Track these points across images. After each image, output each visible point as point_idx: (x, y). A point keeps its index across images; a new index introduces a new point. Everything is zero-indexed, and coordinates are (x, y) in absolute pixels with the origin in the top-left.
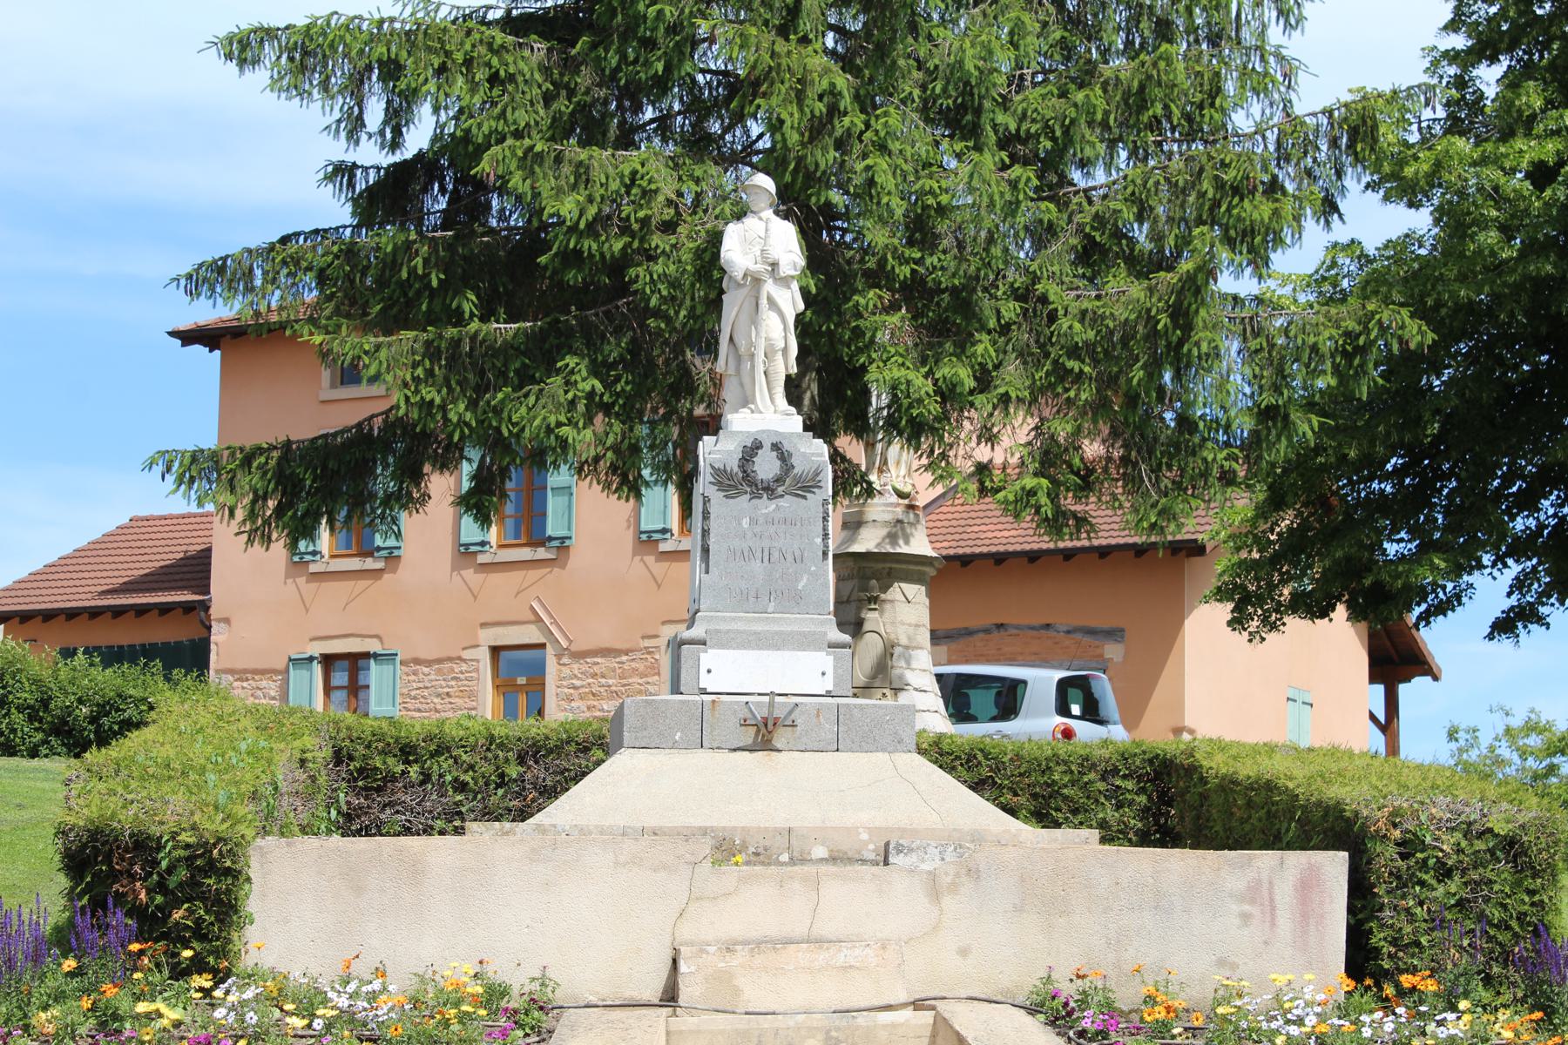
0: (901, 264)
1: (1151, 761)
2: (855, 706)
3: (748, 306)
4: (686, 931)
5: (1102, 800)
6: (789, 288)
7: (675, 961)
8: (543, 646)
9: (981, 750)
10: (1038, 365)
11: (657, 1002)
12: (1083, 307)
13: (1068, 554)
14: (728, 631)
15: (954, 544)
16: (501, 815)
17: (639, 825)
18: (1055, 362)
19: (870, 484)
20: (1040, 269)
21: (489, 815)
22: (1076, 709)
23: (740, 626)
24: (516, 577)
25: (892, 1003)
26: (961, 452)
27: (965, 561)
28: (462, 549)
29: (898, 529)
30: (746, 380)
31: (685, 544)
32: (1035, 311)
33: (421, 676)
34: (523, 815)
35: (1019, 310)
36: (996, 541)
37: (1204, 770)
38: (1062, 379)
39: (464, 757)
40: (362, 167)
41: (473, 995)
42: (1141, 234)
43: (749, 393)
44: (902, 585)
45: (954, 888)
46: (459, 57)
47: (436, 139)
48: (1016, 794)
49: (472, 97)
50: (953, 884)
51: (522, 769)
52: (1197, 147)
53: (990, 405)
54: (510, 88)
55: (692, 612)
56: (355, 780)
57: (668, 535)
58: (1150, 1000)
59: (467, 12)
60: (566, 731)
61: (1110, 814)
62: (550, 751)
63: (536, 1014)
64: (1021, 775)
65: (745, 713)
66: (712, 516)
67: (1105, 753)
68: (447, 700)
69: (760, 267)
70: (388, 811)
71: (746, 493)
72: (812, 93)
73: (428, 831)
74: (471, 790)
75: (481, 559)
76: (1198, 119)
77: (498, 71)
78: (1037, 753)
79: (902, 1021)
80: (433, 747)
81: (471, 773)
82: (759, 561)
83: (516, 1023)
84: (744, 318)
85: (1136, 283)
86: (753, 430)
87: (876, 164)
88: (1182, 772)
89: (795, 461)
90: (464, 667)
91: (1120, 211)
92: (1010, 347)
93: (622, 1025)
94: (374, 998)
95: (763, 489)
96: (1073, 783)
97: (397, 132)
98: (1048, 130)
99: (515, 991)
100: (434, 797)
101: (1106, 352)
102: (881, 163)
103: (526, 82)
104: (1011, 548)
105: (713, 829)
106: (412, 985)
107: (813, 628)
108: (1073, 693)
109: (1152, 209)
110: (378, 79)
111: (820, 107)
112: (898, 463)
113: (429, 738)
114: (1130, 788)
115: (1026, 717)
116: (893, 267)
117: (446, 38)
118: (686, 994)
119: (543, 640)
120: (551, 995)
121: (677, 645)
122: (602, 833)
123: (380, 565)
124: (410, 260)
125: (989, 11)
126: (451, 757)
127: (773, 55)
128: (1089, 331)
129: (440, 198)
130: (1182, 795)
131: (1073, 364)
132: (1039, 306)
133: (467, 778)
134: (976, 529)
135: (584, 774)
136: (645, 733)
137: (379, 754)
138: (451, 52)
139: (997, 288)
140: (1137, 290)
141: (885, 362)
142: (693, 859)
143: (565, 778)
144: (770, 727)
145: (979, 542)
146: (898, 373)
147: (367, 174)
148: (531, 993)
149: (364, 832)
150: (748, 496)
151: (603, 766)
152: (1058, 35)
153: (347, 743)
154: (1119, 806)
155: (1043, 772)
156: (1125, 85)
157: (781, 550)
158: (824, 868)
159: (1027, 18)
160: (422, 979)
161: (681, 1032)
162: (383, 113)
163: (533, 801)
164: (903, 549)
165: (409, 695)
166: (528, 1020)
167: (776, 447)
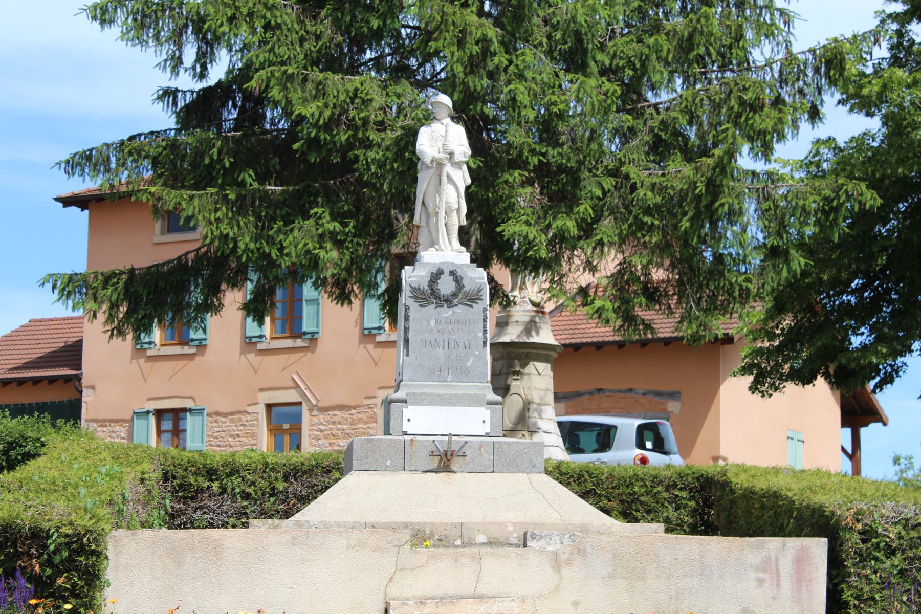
1: (698, 479)
2: (504, 442)
3: (434, 180)
4: (394, 591)
5: (666, 504)
6: (461, 169)
8: (300, 404)
9: (587, 472)
12: (654, 181)
14: (422, 394)
15: (569, 336)
16: (273, 515)
17: (363, 521)
18: (636, 217)
21: (265, 514)
22: (649, 445)
24: (282, 358)
28: (247, 340)
30: (433, 229)
31: (393, 337)
33: (220, 424)
34: (287, 515)
36: (597, 335)
37: (733, 485)
39: (249, 477)
40: (182, 91)
43: (435, 238)
45: (569, 562)
46: (245, 11)
47: (229, 72)
48: (610, 501)
50: (569, 559)
51: (286, 485)
54: (278, 32)
55: (398, 381)
56: (177, 492)
61: (671, 513)
62: (305, 473)
64: (613, 488)
66: (411, 319)
68: (238, 439)
69: (442, 156)
70: (198, 512)
71: (433, 303)
73: (225, 525)
74: (253, 499)
75: (260, 347)
76: (728, 55)
77: (270, 21)
78: (624, 474)
80: (228, 470)
81: (253, 487)
82: (441, 348)
84: (431, 189)
86: (438, 262)
88: (719, 486)
89: (465, 282)
90: (249, 417)
95: (444, 301)
96: (647, 493)
97: (204, 67)
100: (229, 503)
103: (289, 30)
107: (477, 392)
108: (647, 434)
110: (192, 33)
114: (684, 496)
116: (527, 157)
119: (300, 400)
122: (339, 526)
123: (193, 351)
128: (657, 197)
130: (719, 501)
133: (250, 490)
135: (327, 488)
136: (367, 461)
137: (193, 475)
140: (688, 170)
144: (449, 456)
145: (586, 335)
147: (185, 95)
149: (183, 526)
150: (434, 306)
151: (340, 482)
153: (172, 467)
154: (677, 508)
157: (456, 341)
158: (485, 549)
163: (294, 505)
165: (212, 436)
167: (452, 273)
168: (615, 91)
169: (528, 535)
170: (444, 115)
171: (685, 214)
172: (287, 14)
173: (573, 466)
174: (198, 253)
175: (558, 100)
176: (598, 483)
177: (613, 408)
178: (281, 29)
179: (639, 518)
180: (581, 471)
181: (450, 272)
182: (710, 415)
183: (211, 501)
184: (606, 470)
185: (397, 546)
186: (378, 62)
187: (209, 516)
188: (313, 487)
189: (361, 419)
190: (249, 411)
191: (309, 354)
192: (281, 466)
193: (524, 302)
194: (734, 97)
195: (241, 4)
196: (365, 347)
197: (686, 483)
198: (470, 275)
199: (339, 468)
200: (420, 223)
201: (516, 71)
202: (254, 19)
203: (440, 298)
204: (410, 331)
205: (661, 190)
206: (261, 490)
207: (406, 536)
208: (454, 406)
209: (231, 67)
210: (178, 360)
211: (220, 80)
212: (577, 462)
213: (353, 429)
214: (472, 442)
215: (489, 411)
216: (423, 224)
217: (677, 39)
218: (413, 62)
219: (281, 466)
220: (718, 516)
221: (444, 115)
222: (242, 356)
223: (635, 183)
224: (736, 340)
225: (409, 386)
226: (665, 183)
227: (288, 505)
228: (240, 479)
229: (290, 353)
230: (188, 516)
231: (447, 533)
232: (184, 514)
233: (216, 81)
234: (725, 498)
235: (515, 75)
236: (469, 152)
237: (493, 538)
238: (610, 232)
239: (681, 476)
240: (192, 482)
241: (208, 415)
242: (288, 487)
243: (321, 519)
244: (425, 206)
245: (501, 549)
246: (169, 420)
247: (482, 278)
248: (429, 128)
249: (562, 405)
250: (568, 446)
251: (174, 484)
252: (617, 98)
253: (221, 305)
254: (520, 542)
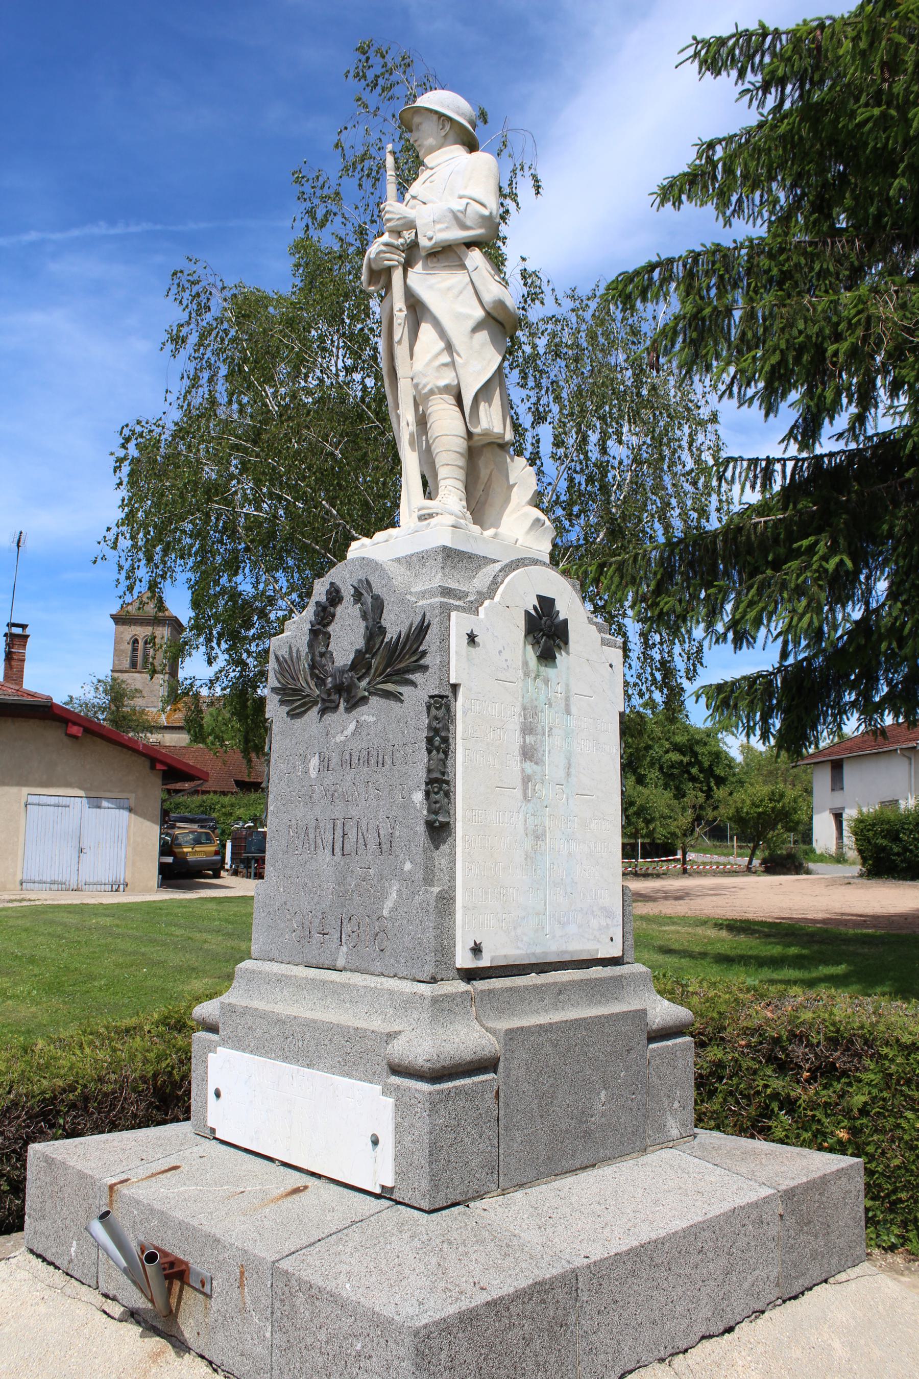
82: (328, 851)
215: (391, 1101)
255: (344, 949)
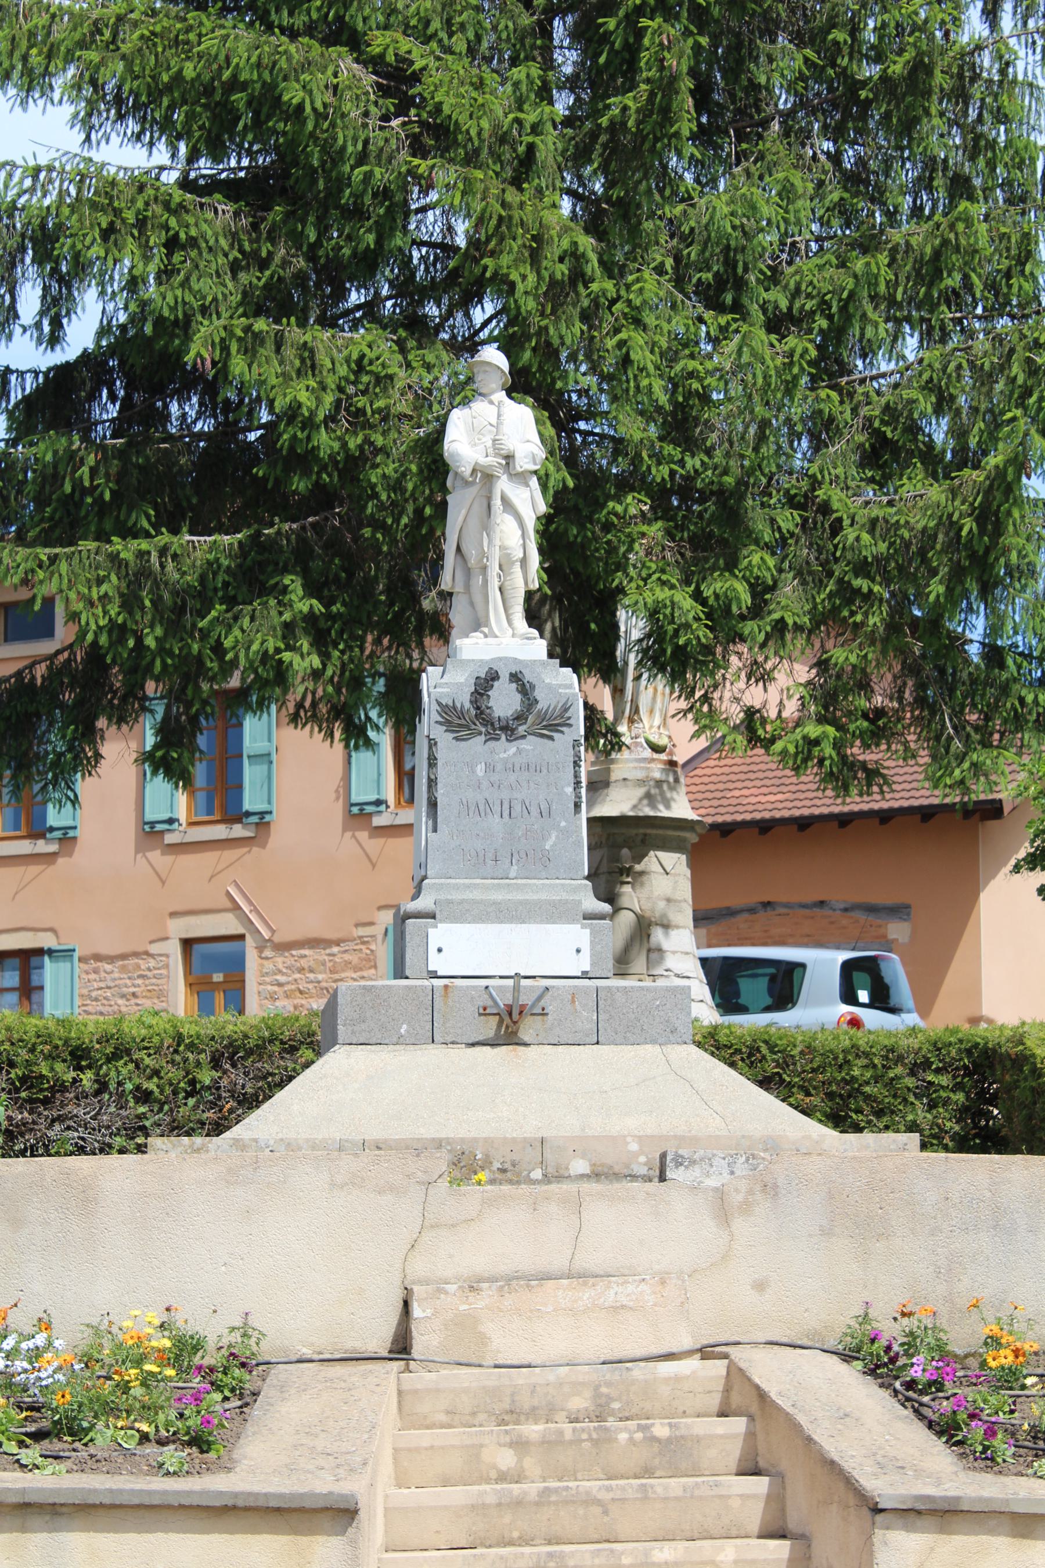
0: (659, 463)
1: (969, 1052)
2: (618, 988)
3: (479, 508)
4: (419, 1267)
5: (912, 1099)
6: (528, 486)
7: (406, 1304)
8: (241, 937)
9: (766, 1042)
10: (820, 585)
11: (386, 1354)
12: (873, 515)
13: (844, 820)
14: (462, 902)
15: (712, 811)
16: (193, 1130)
17: (359, 1138)
18: (840, 581)
19: (617, 735)
20: (821, 471)
21: (177, 1128)
22: (863, 996)
23: (476, 895)
24: (209, 858)
25: (675, 1350)
26: (727, 695)
27: (725, 830)
28: (147, 828)
29: (656, 791)
30: (478, 599)
31: (406, 816)
32: (815, 523)
33: (103, 974)
34: (218, 1128)
35: (798, 520)
36: (760, 807)
37: (1038, 1060)
38: (850, 602)
39: (147, 1061)
40: (17, 371)
41: (159, 1351)
42: (939, 431)
43: (481, 613)
44: (660, 854)
45: (746, 1208)
46: (130, 216)
47: (103, 331)
48: (808, 1094)
49: (146, 265)
50: (746, 1202)
51: (216, 1074)
52: (1003, 323)
53: (763, 634)
54: (194, 254)
55: (416, 881)
56: (17, 1090)
57: (383, 807)
58: (993, 1342)
59: (136, 173)
60: (268, 1028)
61: (921, 1114)
62: (250, 1052)
63: (237, 1373)
64: (813, 1070)
65: (484, 1000)
66: (440, 763)
67: (911, 1041)
68: (133, 1001)
69: (492, 460)
70: (57, 1127)
71: (480, 733)
72: (552, 253)
73: (105, 1149)
74: (159, 1101)
75: (169, 839)
76: (1005, 290)
77: (177, 234)
78: (833, 1045)
79: (688, 1372)
80: (109, 1050)
81: (155, 1080)
82: (497, 816)
83: (212, 1384)
84: (473, 523)
85: (936, 485)
86: (487, 657)
87: (630, 337)
88: (1008, 1064)
89: (538, 694)
90: (152, 963)
91: (914, 401)
92: (786, 565)
93: (343, 1385)
94: (38, 1357)
95: (501, 729)
96: (877, 1079)
97: (57, 324)
98: (824, 305)
99: (211, 1344)
100: (112, 1109)
101: (900, 568)
102: (637, 338)
103: (210, 249)
104: (778, 815)
105: (448, 1141)
106: (84, 1339)
107: (564, 896)
108: (858, 977)
109: (952, 398)
110: (33, 261)
111: (562, 270)
112: (651, 711)
113: (105, 1039)
114: (944, 1083)
115: (805, 1006)
116: (649, 467)
117: (115, 193)
118: (421, 1343)
119: (241, 930)
120: (255, 1348)
121: (403, 919)
122: (314, 1148)
123: (53, 848)
124: (75, 470)
125: (753, 169)
126: (132, 1061)
127: (504, 205)
128: (880, 543)
129: (110, 406)
130: (1008, 1091)
131: (861, 583)
132: (820, 518)
133: (151, 1085)
134: (737, 793)
135: (291, 1079)
136: (363, 1026)
137: (46, 1058)
138: (121, 211)
139: (770, 496)
140: (936, 493)
141: (645, 580)
142: (425, 1178)
143: (269, 1084)
144: (515, 1016)
145: (741, 809)
146: (663, 594)
147: (23, 380)
148: (230, 1346)
149: (30, 1152)
150: (483, 738)
151: (313, 1067)
152: (835, 196)
153: (7, 1046)
154: (932, 1106)
155: (841, 1066)
156: (917, 253)
157: (523, 802)
158: (587, 1186)
159: (796, 178)
160: (96, 1331)
161: (416, 1391)
162: (39, 301)
163: (231, 1111)
164: (664, 813)
165: (90, 997)
166: (227, 1380)
167: (515, 677)
168: (806, 351)
169: (669, 1158)
170: (494, 386)
171: (934, 572)
172: (206, 221)
173: (739, 1032)
174: (52, 663)
175: (700, 368)
176: (785, 1062)
177: (791, 936)
178: (199, 248)
179: (863, 1124)
180: (755, 1041)
181: (511, 675)
182: (962, 944)
183: (79, 1105)
184: (800, 1038)
185: (423, 1183)
186: (371, 308)
187: (76, 1134)
188: (265, 1078)
189: (348, 963)
190: (152, 951)
191: (255, 849)
192: (206, 1041)
193: (637, 744)
194: (1018, 360)
195: (123, 205)
196: (354, 836)
197: (948, 1060)
198: (547, 681)
199: (312, 1042)
200: (453, 586)
201: (627, 310)
202: (146, 230)
203: (492, 724)
204: (439, 786)
205: (888, 530)
206: (171, 1084)
207: (441, 1163)
208: (524, 922)
209: (105, 322)
210: (27, 864)
211: (85, 350)
212: (745, 1025)
213: (336, 981)
214: (558, 988)
215: (588, 931)
216: (459, 588)
217: (911, 260)
218: (432, 310)
219: (206, 1041)
220: (1008, 1118)
221: (494, 386)
222: (139, 856)
223: (840, 520)
224: (1007, 809)
225: (439, 888)
226: (896, 518)
227: (220, 1111)
228: (131, 1066)
229: (223, 849)
230: (39, 1134)
231: (515, 1157)
232: (31, 1130)
233: (79, 353)
234: (1022, 1084)
235: (626, 319)
236: (541, 454)
237: (602, 1165)
238: (796, 607)
239: (937, 1047)
240: (44, 1072)
241: (80, 960)
242: (220, 1078)
243: (280, 1136)
244: (462, 556)
245: (617, 1185)
246: (14, 969)
247: (571, 686)
248: (466, 411)
249: (703, 931)
250: (718, 1000)
251: (12, 1076)
252: (810, 363)
253: (98, 756)
254: (651, 1172)
255: (515, 867)
